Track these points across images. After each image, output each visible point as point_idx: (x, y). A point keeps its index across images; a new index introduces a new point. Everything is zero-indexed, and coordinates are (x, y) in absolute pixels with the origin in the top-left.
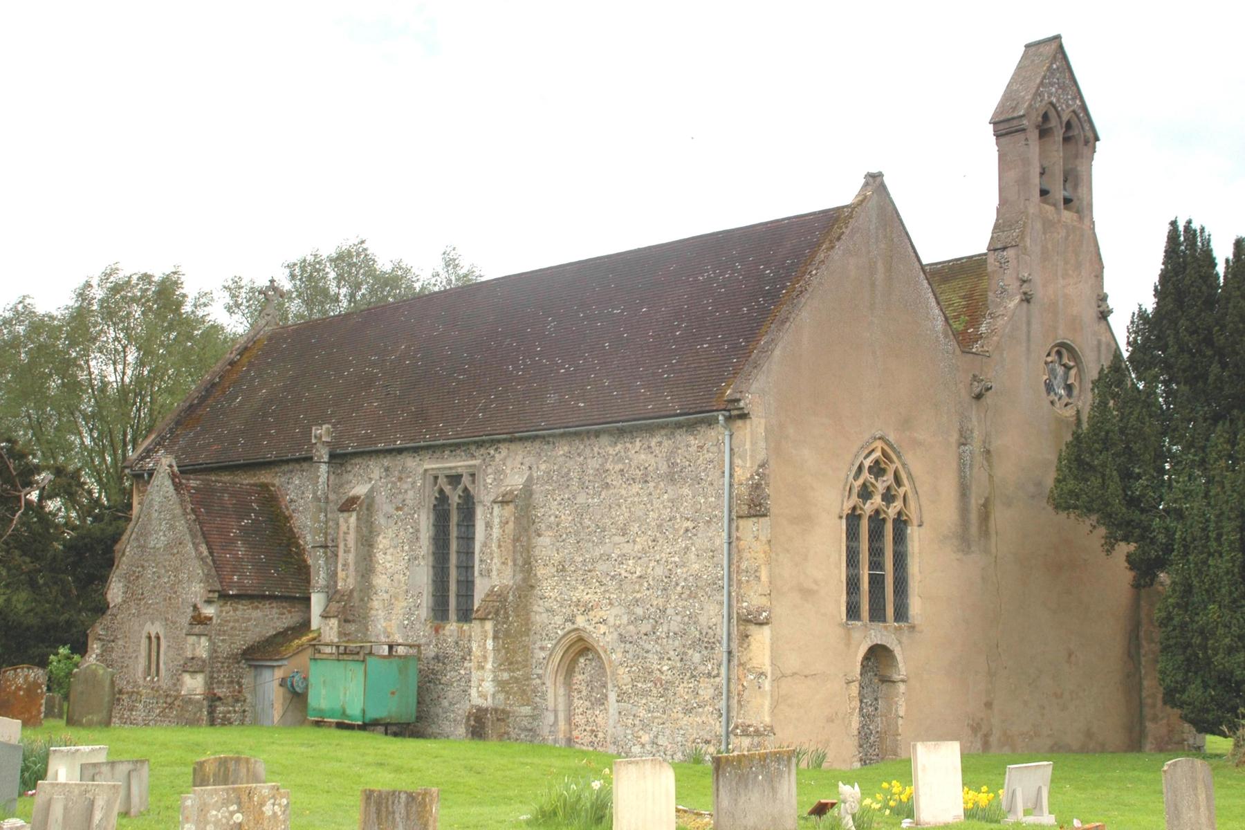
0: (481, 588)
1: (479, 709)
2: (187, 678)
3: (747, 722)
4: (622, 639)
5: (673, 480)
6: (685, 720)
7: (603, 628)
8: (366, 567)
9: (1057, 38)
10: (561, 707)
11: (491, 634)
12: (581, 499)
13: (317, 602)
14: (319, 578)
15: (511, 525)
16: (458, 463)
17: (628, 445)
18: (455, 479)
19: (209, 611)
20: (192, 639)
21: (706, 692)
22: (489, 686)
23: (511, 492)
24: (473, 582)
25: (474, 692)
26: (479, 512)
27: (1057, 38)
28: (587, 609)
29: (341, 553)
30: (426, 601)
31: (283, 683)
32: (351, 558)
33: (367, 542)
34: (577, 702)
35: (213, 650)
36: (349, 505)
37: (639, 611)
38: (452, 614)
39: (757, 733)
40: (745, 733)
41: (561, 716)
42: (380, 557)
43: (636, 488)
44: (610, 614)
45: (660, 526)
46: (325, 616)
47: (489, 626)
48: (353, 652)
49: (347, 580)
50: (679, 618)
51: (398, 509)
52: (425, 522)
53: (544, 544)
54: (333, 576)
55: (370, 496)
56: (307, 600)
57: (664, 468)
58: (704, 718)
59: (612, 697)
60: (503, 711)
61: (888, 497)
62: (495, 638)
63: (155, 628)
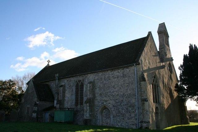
0: (85, 99)
1: (86, 119)
2: (33, 114)
3: (145, 121)
4: (114, 106)
5: (124, 77)
6: (128, 121)
7: (109, 104)
8: (64, 96)
9: (164, 23)
10: (101, 119)
11: (88, 106)
12: (104, 82)
13: (55, 102)
14: (56, 98)
15: (91, 87)
16: (81, 78)
17: (114, 72)
18: (79, 81)
19: (38, 103)
20: (35, 107)
21: (133, 115)
22: (88, 115)
23: (91, 81)
24: (83, 98)
25: (85, 117)
26: (85, 86)
27: (164, 23)
28: (106, 101)
29: (60, 94)
30: (74, 101)
31: (50, 115)
32: (61, 95)
33: (64, 92)
34: (103, 118)
35: (38, 109)
36: (62, 86)
37: (117, 101)
38: (79, 104)
39: (147, 122)
40: (145, 123)
41: (101, 121)
42: (66, 95)
43: (116, 79)
44: (111, 102)
45: (121, 85)
46: (57, 104)
47: (88, 104)
48: (62, 109)
49: (60, 98)
50: (126, 102)
51: (69, 87)
52: (74, 88)
53: (97, 91)
54: (58, 98)
55: (65, 85)
56: (54, 102)
57: (122, 75)
58: (132, 120)
59: (112, 117)
60: (90, 120)
61: (156, 82)
62: (89, 106)
63: (28, 106)
